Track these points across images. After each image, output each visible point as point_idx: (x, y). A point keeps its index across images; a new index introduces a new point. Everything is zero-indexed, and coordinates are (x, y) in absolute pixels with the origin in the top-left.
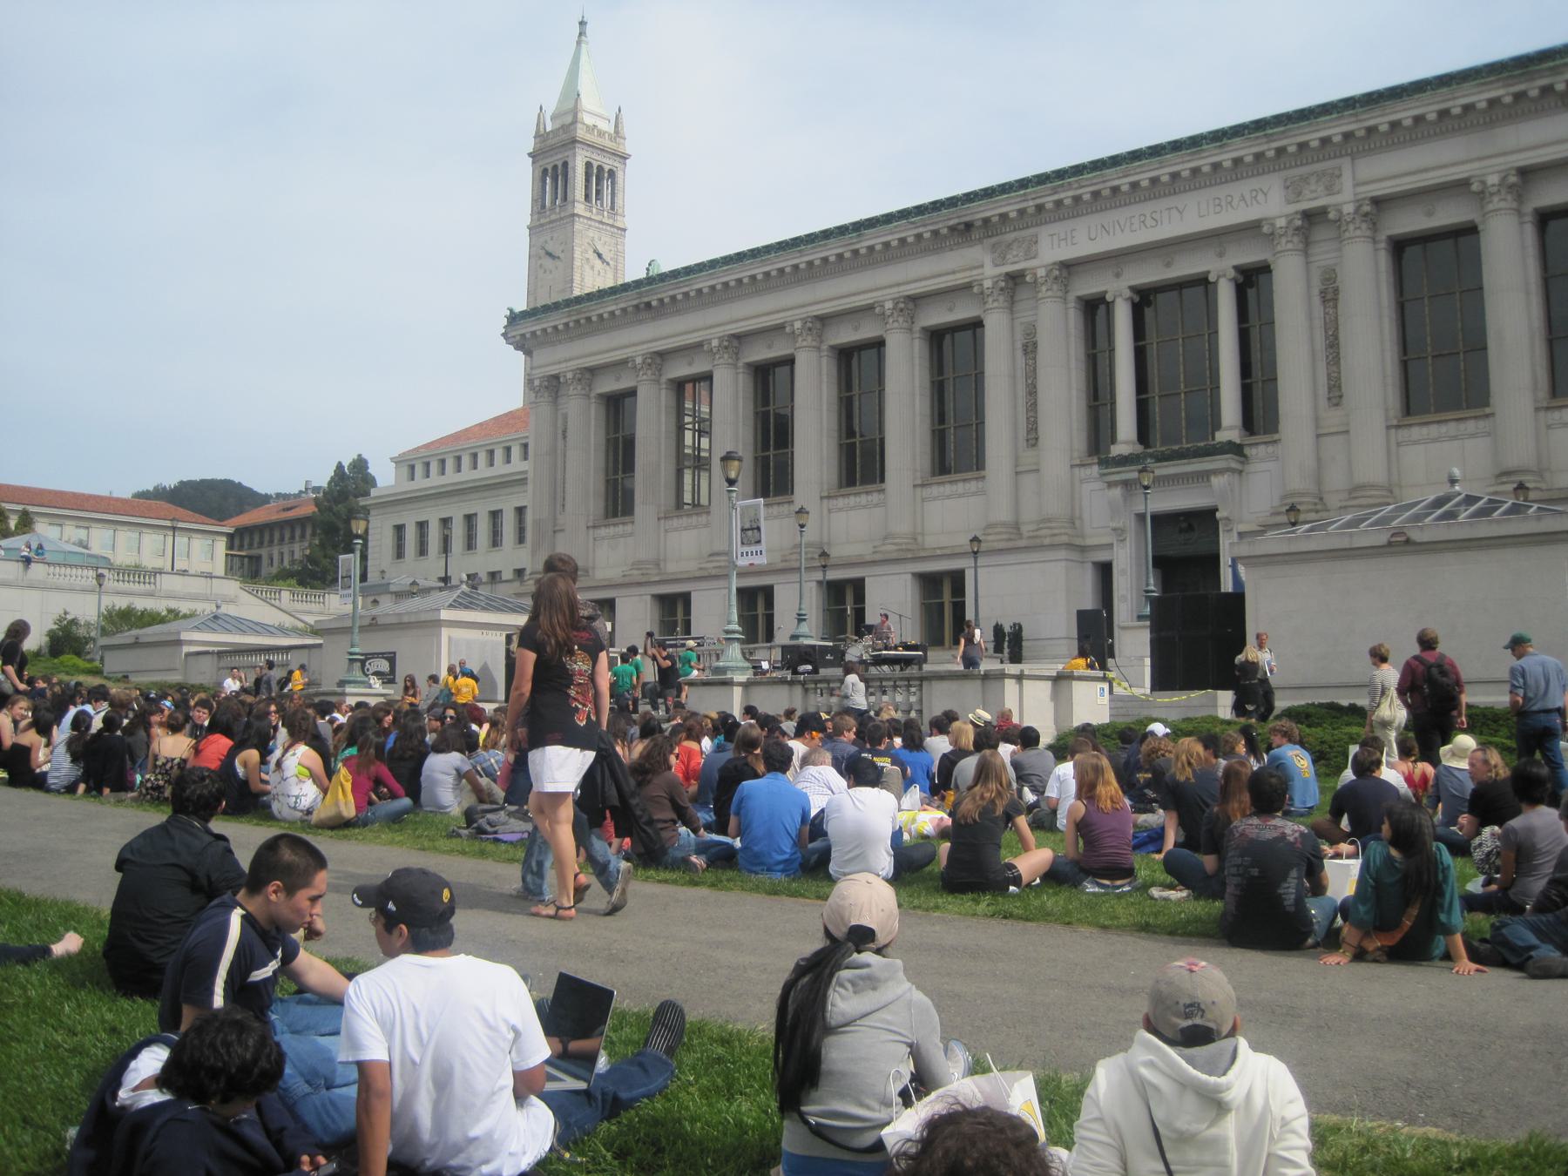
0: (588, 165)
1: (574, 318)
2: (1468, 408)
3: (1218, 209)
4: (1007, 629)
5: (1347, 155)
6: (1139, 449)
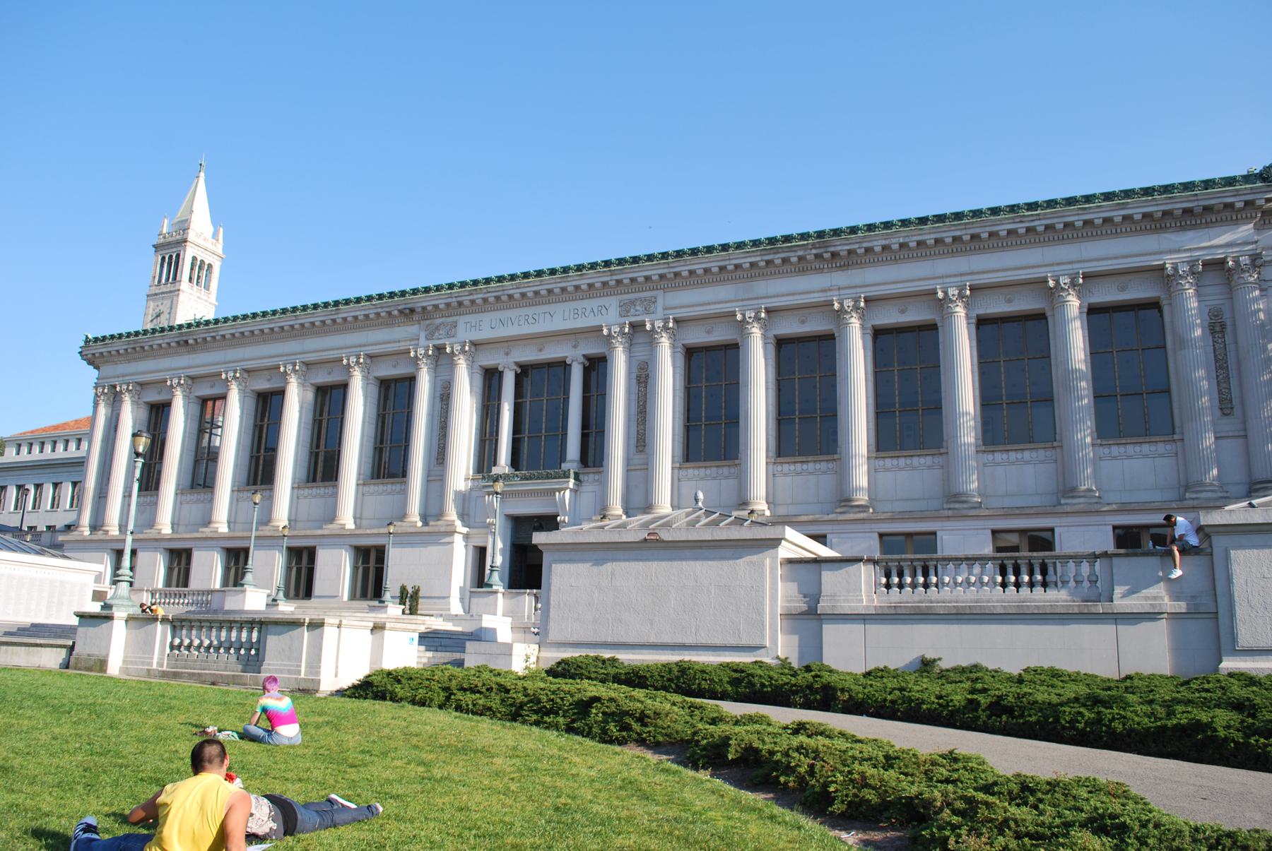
0: (194, 258)
1: (132, 346)
2: (900, 450)
3: (576, 316)
4: (410, 591)
5: (661, 289)
6: (513, 471)
